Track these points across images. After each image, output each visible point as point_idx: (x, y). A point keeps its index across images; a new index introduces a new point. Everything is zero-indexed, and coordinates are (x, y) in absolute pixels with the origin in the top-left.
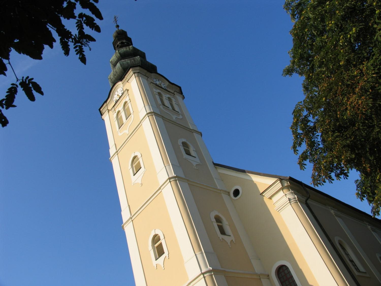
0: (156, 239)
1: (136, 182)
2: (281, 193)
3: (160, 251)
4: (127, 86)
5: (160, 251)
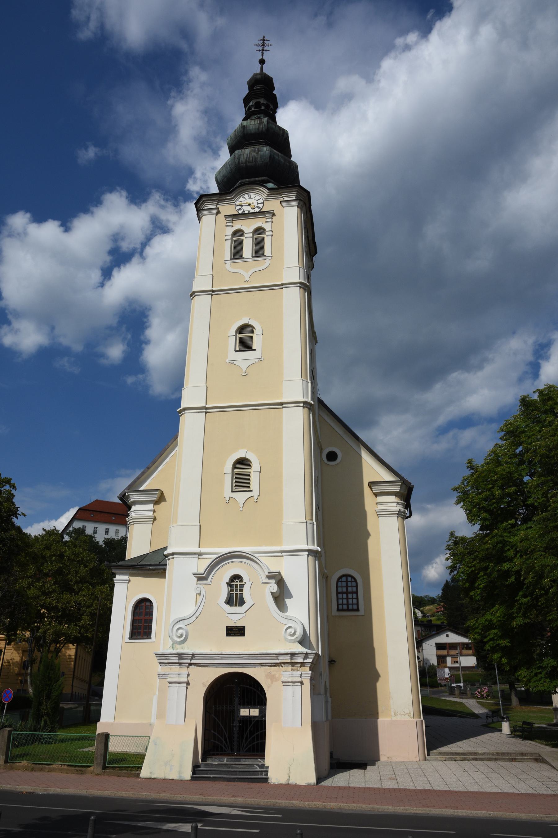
0: (246, 328)
1: (235, 363)
2: (393, 498)
3: (245, 345)
4: (273, 204)
5: (245, 345)
